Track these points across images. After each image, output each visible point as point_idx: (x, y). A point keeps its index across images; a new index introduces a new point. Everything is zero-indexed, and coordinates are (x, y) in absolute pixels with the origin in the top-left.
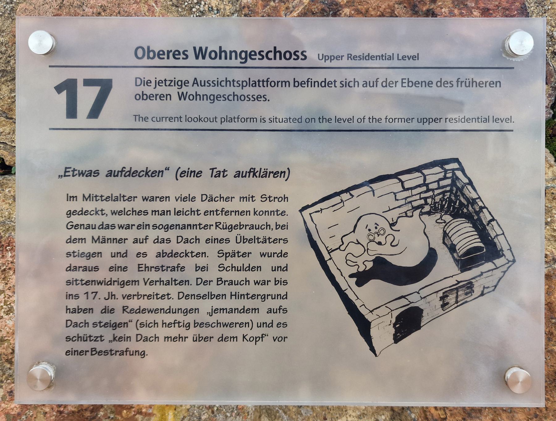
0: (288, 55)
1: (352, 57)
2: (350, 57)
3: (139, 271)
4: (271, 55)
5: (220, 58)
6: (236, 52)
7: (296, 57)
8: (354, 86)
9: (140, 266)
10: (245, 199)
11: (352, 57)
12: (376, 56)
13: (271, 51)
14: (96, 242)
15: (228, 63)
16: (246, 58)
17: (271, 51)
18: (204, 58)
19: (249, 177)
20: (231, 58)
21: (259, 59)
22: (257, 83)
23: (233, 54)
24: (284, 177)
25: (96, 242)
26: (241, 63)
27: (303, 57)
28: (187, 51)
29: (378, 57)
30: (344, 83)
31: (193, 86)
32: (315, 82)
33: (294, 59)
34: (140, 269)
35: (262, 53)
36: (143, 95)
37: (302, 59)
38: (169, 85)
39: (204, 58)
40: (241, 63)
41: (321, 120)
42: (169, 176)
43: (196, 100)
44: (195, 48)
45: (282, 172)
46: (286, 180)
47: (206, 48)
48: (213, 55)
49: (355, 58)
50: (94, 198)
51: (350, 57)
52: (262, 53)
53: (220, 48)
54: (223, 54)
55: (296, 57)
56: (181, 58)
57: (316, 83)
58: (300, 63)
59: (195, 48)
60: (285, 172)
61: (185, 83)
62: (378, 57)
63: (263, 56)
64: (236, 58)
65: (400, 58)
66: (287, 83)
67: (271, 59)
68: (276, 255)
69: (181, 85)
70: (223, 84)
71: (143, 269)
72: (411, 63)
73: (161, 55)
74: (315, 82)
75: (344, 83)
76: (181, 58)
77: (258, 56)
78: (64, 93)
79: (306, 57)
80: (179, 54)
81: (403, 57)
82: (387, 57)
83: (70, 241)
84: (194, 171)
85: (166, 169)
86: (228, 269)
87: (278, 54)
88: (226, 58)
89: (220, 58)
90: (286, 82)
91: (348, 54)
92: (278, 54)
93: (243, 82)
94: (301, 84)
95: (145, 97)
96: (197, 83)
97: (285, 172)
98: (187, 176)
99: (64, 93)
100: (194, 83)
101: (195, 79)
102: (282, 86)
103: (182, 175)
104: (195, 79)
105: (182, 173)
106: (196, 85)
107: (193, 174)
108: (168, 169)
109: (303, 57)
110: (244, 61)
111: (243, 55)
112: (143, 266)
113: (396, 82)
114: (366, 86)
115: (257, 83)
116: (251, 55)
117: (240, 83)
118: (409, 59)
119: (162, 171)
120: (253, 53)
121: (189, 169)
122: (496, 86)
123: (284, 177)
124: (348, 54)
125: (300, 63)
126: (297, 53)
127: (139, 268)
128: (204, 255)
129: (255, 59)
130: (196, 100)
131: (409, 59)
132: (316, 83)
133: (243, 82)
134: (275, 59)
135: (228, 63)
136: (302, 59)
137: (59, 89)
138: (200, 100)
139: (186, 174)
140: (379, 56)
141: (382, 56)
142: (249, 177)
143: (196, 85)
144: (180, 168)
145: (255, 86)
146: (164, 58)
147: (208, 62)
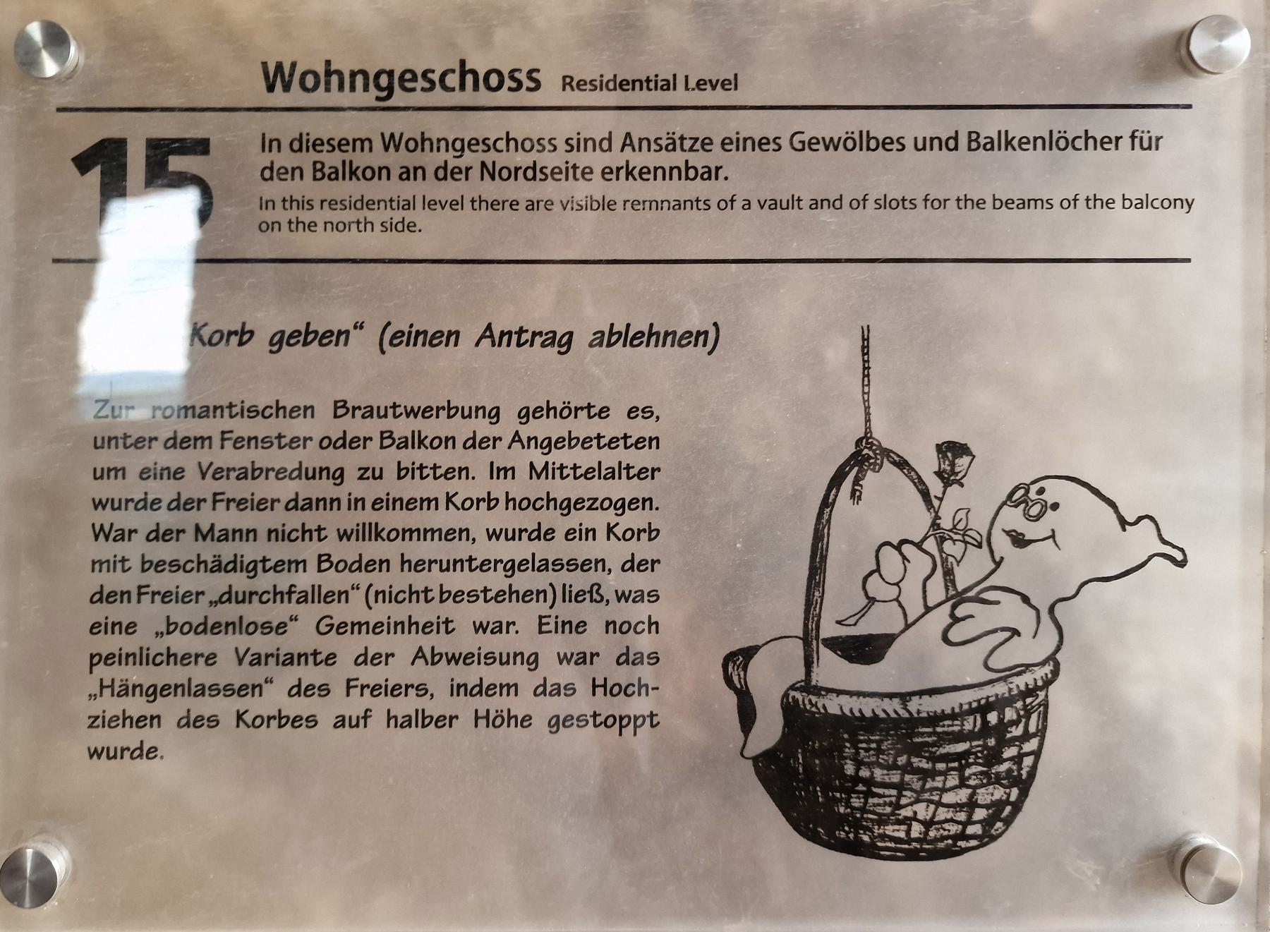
0: (494, 81)
1: (574, 84)
2: (570, 84)
3: (541, 632)
4: (453, 80)
5: (328, 90)
6: (364, 73)
7: (514, 85)
8: (1086, 148)
9: (544, 620)
10: (436, 535)
11: (574, 84)
12: (634, 82)
13: (453, 71)
14: (204, 538)
15: (345, 99)
16: (390, 89)
17: (453, 71)
18: (287, 87)
19: (508, 345)
20: (353, 88)
21: (423, 89)
22: (678, 142)
23: (359, 79)
24: (705, 345)
25: (204, 538)
26: (378, 99)
27: (532, 85)
28: (538, 71)
29: (637, 84)
30: (574, 143)
31: (348, 695)
32: (271, 141)
33: (510, 89)
34: (544, 628)
35: (430, 75)
36: (687, 169)
37: (529, 89)
38: (691, 149)
39: (287, 87)
40: (378, 99)
41: (293, 226)
42: (362, 344)
43: (380, 178)
44: (265, 65)
45: (340, 333)
46: (710, 353)
47: (294, 65)
48: (310, 81)
49: (581, 85)
50: (557, 472)
51: (570, 84)
52: (430, 75)
53: (328, 63)
54: (335, 78)
55: (514, 85)
56: (419, 89)
57: (590, 143)
58: (524, 98)
59: (265, 65)
60: (706, 333)
61: (469, 144)
62: (637, 84)
63: (432, 82)
64: (366, 88)
65: (692, 84)
66: (367, 144)
67: (453, 89)
68: (127, 754)
69: (462, 149)
70: (1080, 143)
71: (552, 627)
72: (719, 97)
73: (409, 80)
74: (745, 140)
75: (574, 143)
76: (419, 89)
77: (421, 83)
78: (95, 174)
79: (537, 82)
80: (414, 79)
81: (698, 84)
82: (660, 84)
83: (100, 475)
84: (425, 332)
85: (355, 327)
86: (189, 567)
87: (469, 78)
88: (341, 87)
89: (328, 90)
90: (362, 141)
91: (970, 133)
92: (469, 78)
93: (534, 178)
94: (884, 144)
95: (692, 173)
96: (631, 144)
97: (706, 333)
98: (408, 344)
99: (95, 174)
100: (624, 145)
101: (628, 135)
102: (362, 150)
103: (396, 342)
104: (628, 135)
105: (394, 337)
106: (628, 149)
107: (670, 339)
108: (361, 327)
109: (532, 85)
110: (385, 94)
111: (384, 81)
112: (552, 621)
113: (1118, 139)
114: (674, 149)
115: (678, 142)
116: (407, 78)
117: (539, 175)
118: (714, 88)
119: (347, 332)
120: (408, 76)
121: (411, 326)
122: (1035, 148)
123: (705, 345)
124: (970, 133)
125: (524, 98)
126: (517, 75)
127: (541, 624)
128: (648, 503)
129: (413, 90)
130: (380, 178)
131: (714, 88)
132: (590, 143)
133: (534, 178)
134: (463, 86)
135: (345, 99)
136: (529, 89)
137: (83, 163)
138: (664, 179)
139: (405, 339)
140: (640, 81)
141: (648, 80)
142: (508, 345)
143: (628, 149)
144: (389, 324)
145: (674, 149)
146: (413, 90)
147: (296, 97)
